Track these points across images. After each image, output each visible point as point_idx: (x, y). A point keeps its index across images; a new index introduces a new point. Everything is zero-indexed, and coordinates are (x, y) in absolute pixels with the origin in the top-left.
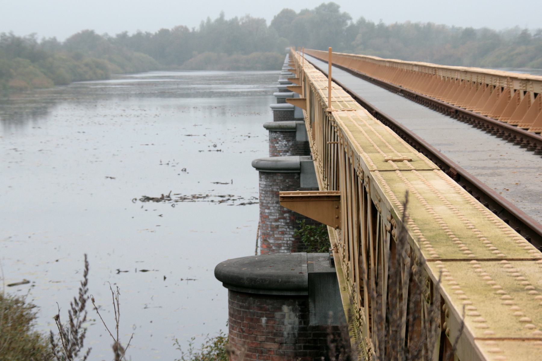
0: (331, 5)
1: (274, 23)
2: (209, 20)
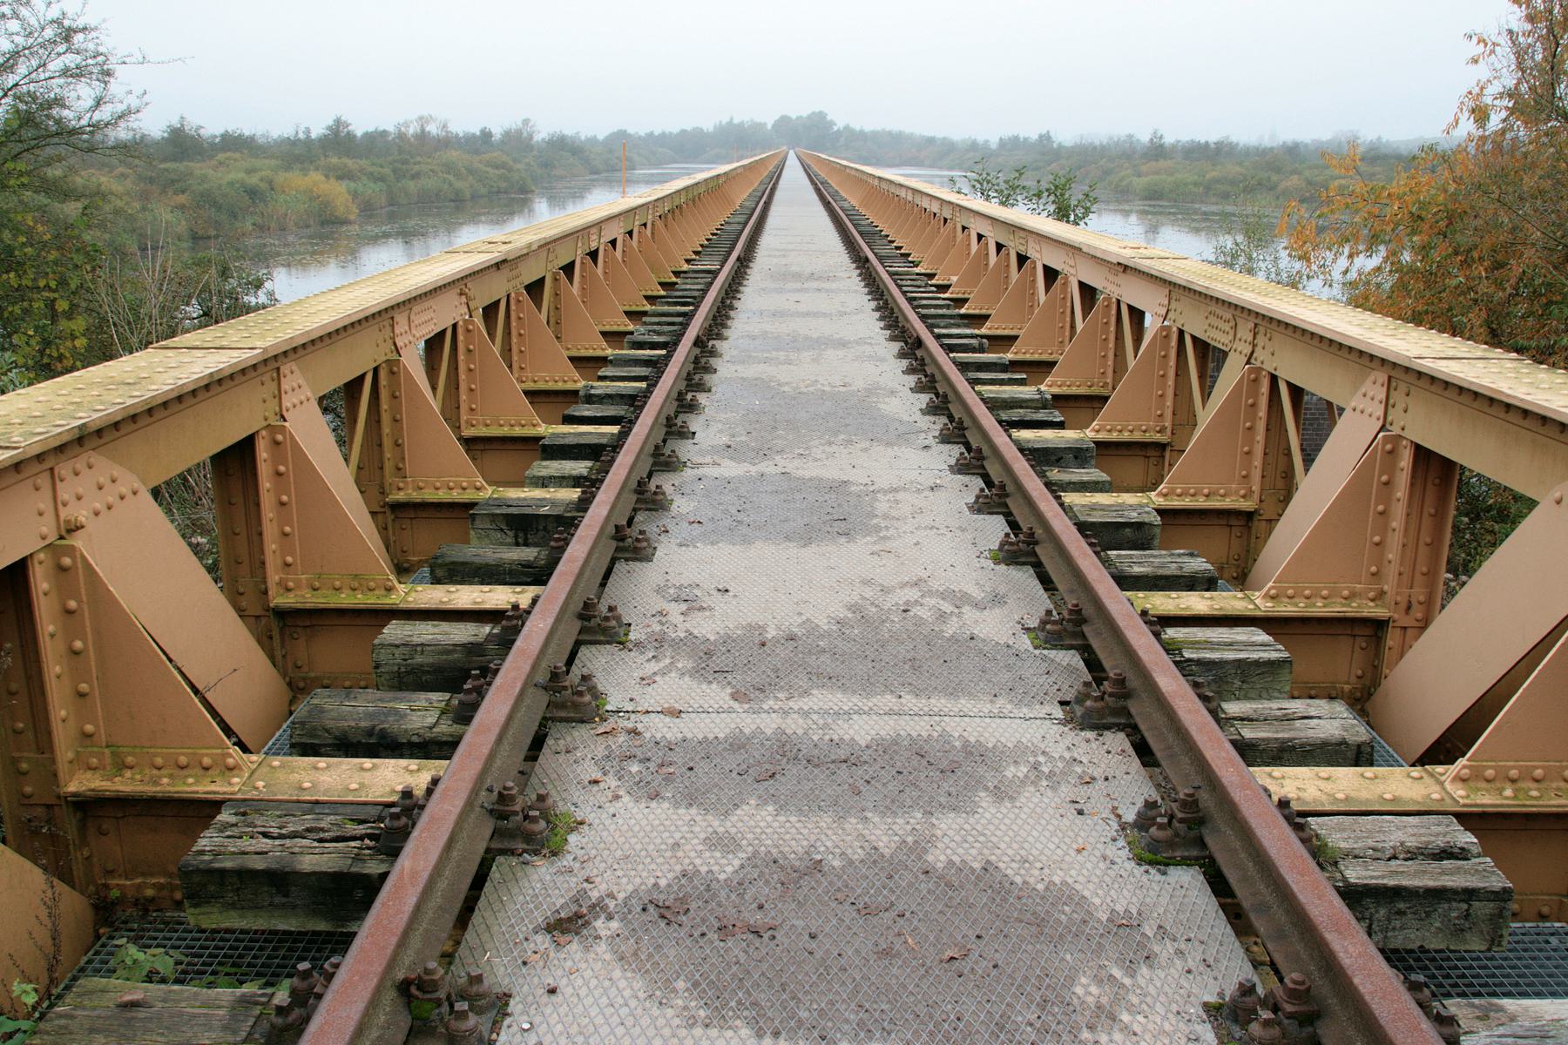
0: (820, 112)
1: (773, 126)
2: (308, 131)
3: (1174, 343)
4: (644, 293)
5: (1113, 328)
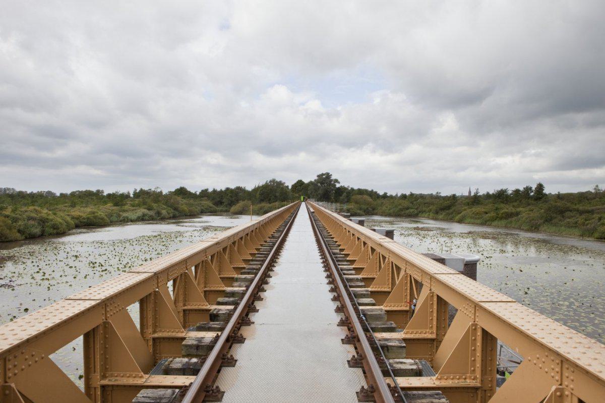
3: (391, 265)
4: (233, 266)
5: (409, 285)
